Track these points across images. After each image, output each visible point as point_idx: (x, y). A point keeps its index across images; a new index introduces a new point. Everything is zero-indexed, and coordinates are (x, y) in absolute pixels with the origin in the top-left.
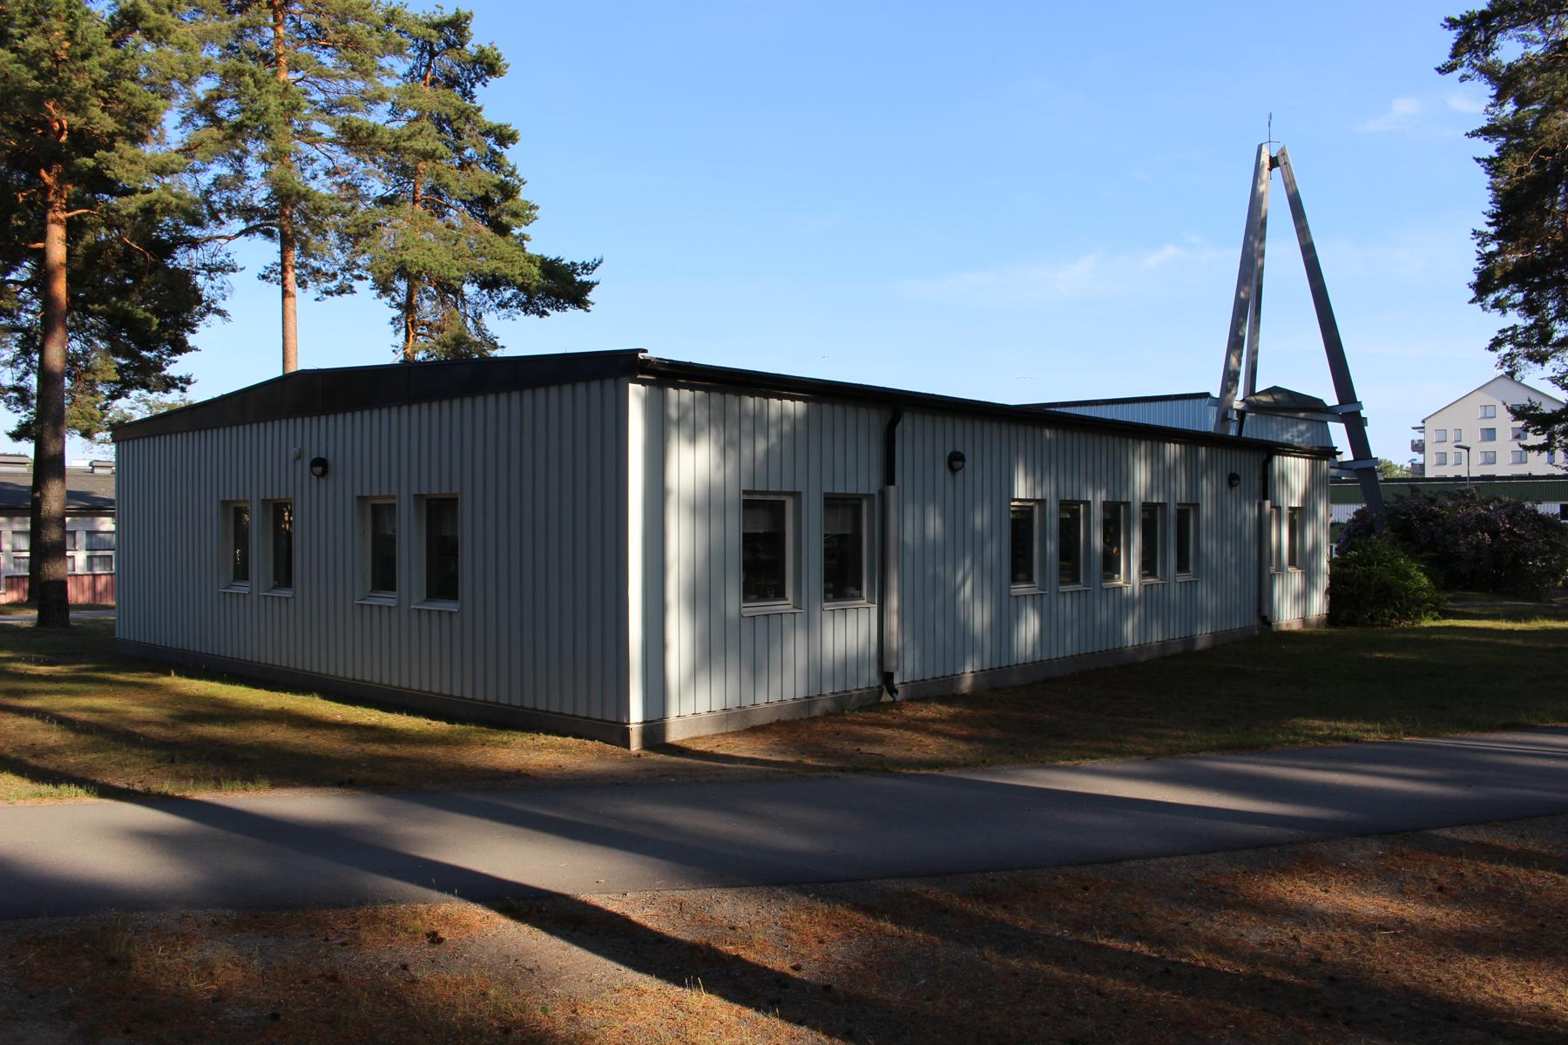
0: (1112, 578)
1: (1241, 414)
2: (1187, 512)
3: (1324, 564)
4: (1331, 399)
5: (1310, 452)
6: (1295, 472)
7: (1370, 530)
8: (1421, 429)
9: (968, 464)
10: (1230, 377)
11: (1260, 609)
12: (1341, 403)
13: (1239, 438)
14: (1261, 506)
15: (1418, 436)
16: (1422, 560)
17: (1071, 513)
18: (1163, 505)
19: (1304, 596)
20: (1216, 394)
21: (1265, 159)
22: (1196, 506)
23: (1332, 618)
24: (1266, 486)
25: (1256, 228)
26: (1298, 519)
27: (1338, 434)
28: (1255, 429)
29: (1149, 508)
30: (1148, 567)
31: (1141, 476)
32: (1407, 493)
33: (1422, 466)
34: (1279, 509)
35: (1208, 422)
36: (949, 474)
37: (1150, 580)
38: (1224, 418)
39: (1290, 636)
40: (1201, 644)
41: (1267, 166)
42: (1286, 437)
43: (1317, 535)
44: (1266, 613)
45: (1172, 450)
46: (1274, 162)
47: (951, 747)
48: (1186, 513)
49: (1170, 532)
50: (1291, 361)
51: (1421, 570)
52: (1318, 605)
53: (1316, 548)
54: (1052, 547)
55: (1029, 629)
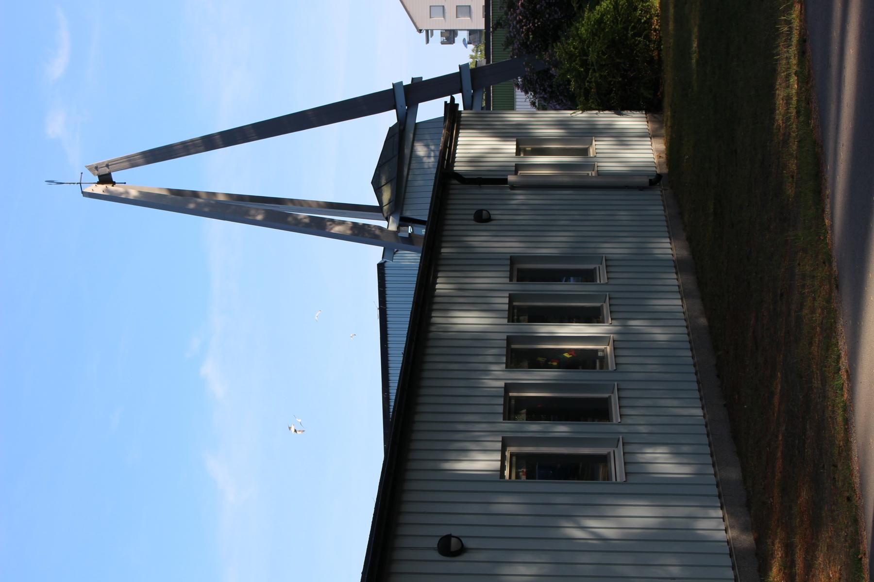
0: (603, 360)
1: (404, 221)
2: (520, 271)
3: (580, 115)
4: (389, 118)
5: (450, 130)
6: (472, 145)
7: (545, 74)
8: (429, 34)
9: (455, 531)
10: (361, 234)
11: (641, 188)
12: (394, 107)
13: (429, 212)
14: (513, 187)
15: (437, 37)
16: (581, 8)
17: (515, 407)
18: (511, 298)
19: (621, 137)
20: (376, 253)
21: (100, 189)
22: (513, 260)
23: (650, 106)
24: (490, 180)
25: (180, 201)
26: (528, 144)
27: (431, 110)
28: (420, 206)
29: (515, 314)
30: (591, 316)
31: (469, 320)
32: (502, 33)
33: (471, 32)
34: (518, 167)
35: (411, 259)
36: (465, 557)
37: (606, 311)
38: (409, 241)
39: (673, 154)
40: (684, 253)
41: (110, 187)
42: (431, 162)
43: (546, 123)
44: (645, 180)
45: (442, 286)
46: (105, 179)
47: (830, 547)
48: (521, 270)
49: (539, 290)
50: (344, 164)
51: (592, 9)
52: (633, 122)
53: (561, 124)
54: (561, 429)
55: (662, 462)
